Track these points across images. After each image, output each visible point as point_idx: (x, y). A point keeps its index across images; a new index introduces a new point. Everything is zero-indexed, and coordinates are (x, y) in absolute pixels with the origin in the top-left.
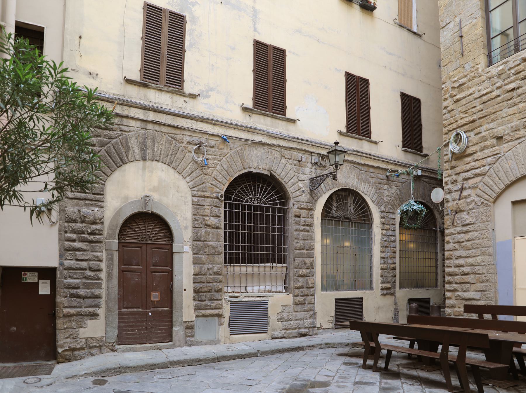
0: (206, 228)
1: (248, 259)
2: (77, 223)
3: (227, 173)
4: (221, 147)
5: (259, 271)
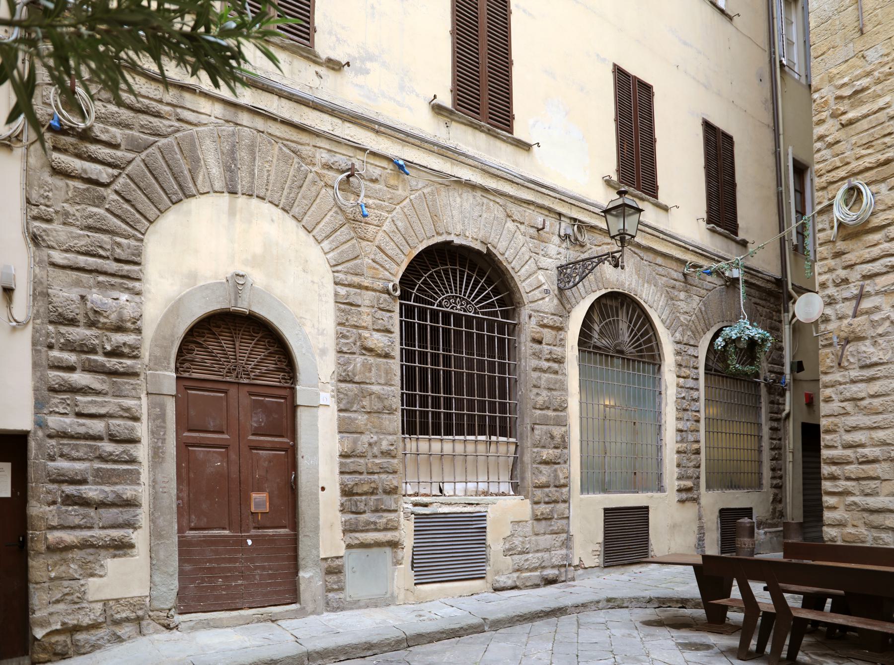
0: (364, 355)
2: (78, 326)
4: (392, 182)
5: (465, 452)
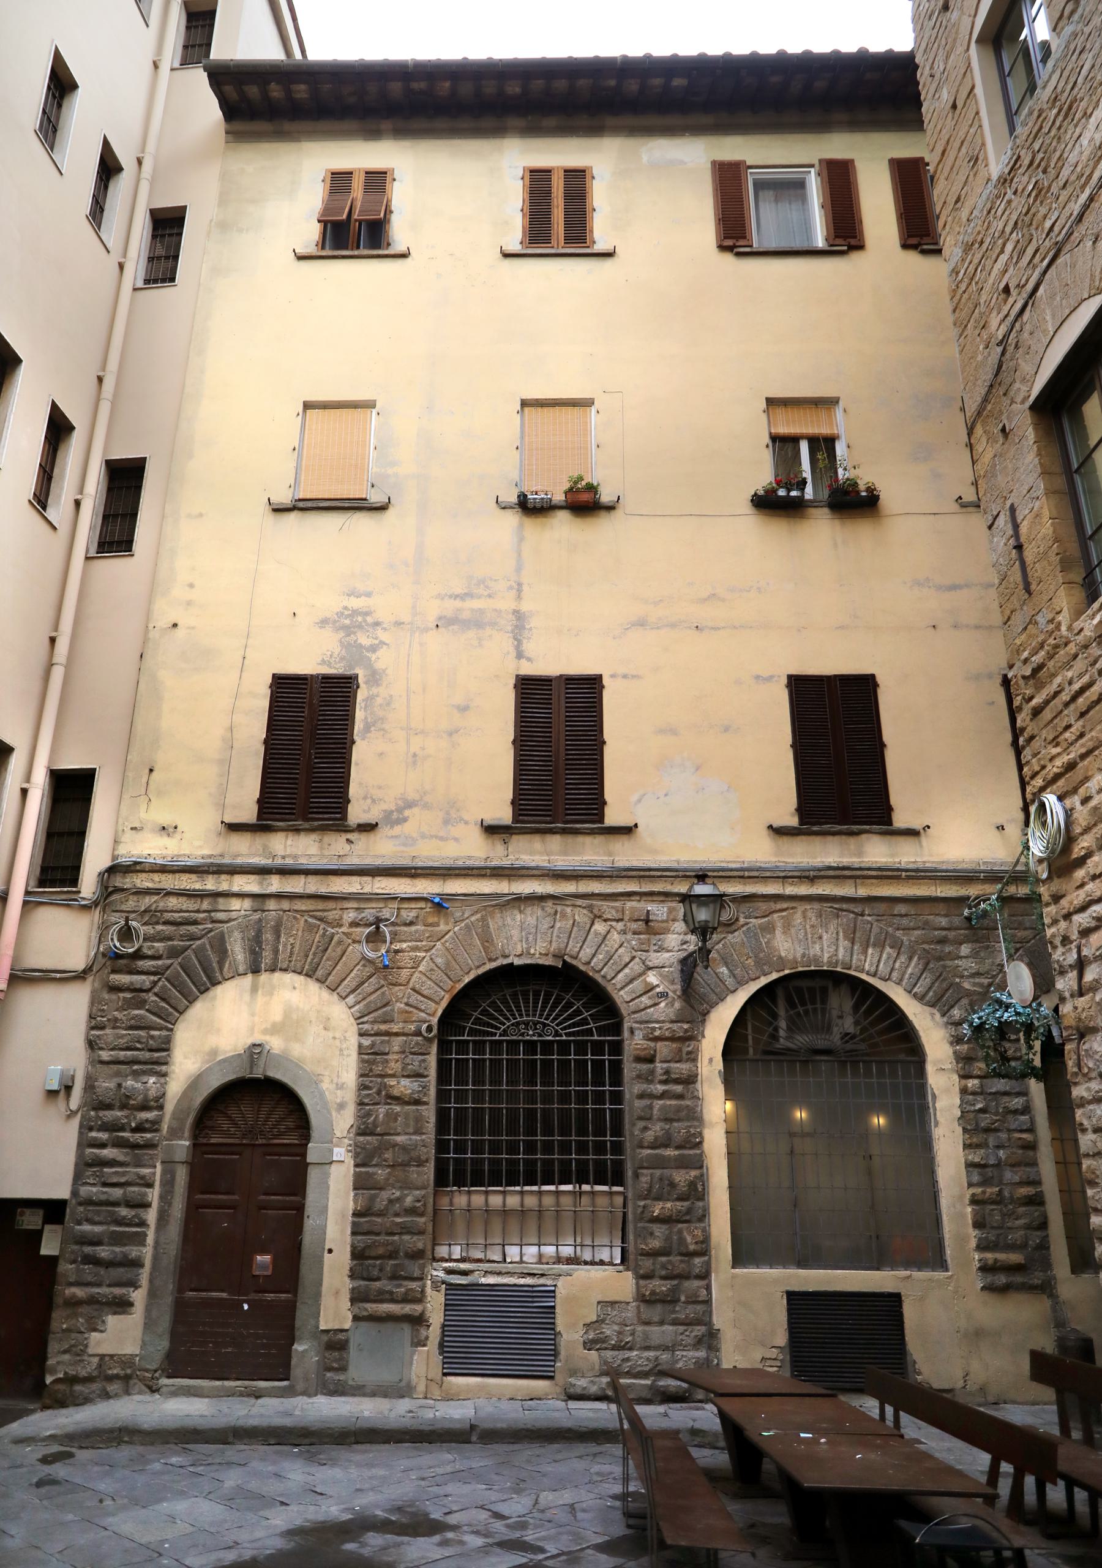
0: (389, 1104)
1: (560, 1172)
2: (113, 1109)
3: (446, 974)
